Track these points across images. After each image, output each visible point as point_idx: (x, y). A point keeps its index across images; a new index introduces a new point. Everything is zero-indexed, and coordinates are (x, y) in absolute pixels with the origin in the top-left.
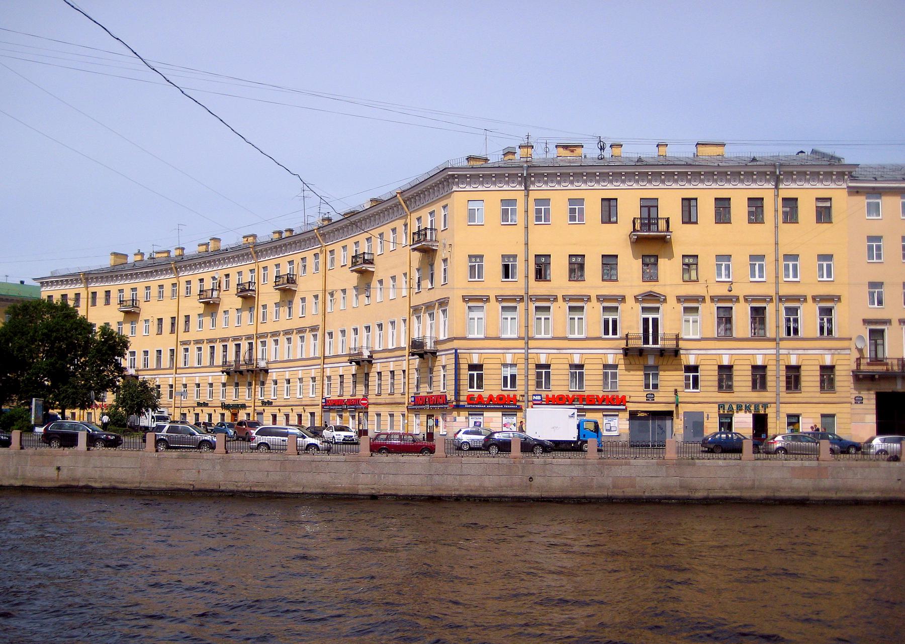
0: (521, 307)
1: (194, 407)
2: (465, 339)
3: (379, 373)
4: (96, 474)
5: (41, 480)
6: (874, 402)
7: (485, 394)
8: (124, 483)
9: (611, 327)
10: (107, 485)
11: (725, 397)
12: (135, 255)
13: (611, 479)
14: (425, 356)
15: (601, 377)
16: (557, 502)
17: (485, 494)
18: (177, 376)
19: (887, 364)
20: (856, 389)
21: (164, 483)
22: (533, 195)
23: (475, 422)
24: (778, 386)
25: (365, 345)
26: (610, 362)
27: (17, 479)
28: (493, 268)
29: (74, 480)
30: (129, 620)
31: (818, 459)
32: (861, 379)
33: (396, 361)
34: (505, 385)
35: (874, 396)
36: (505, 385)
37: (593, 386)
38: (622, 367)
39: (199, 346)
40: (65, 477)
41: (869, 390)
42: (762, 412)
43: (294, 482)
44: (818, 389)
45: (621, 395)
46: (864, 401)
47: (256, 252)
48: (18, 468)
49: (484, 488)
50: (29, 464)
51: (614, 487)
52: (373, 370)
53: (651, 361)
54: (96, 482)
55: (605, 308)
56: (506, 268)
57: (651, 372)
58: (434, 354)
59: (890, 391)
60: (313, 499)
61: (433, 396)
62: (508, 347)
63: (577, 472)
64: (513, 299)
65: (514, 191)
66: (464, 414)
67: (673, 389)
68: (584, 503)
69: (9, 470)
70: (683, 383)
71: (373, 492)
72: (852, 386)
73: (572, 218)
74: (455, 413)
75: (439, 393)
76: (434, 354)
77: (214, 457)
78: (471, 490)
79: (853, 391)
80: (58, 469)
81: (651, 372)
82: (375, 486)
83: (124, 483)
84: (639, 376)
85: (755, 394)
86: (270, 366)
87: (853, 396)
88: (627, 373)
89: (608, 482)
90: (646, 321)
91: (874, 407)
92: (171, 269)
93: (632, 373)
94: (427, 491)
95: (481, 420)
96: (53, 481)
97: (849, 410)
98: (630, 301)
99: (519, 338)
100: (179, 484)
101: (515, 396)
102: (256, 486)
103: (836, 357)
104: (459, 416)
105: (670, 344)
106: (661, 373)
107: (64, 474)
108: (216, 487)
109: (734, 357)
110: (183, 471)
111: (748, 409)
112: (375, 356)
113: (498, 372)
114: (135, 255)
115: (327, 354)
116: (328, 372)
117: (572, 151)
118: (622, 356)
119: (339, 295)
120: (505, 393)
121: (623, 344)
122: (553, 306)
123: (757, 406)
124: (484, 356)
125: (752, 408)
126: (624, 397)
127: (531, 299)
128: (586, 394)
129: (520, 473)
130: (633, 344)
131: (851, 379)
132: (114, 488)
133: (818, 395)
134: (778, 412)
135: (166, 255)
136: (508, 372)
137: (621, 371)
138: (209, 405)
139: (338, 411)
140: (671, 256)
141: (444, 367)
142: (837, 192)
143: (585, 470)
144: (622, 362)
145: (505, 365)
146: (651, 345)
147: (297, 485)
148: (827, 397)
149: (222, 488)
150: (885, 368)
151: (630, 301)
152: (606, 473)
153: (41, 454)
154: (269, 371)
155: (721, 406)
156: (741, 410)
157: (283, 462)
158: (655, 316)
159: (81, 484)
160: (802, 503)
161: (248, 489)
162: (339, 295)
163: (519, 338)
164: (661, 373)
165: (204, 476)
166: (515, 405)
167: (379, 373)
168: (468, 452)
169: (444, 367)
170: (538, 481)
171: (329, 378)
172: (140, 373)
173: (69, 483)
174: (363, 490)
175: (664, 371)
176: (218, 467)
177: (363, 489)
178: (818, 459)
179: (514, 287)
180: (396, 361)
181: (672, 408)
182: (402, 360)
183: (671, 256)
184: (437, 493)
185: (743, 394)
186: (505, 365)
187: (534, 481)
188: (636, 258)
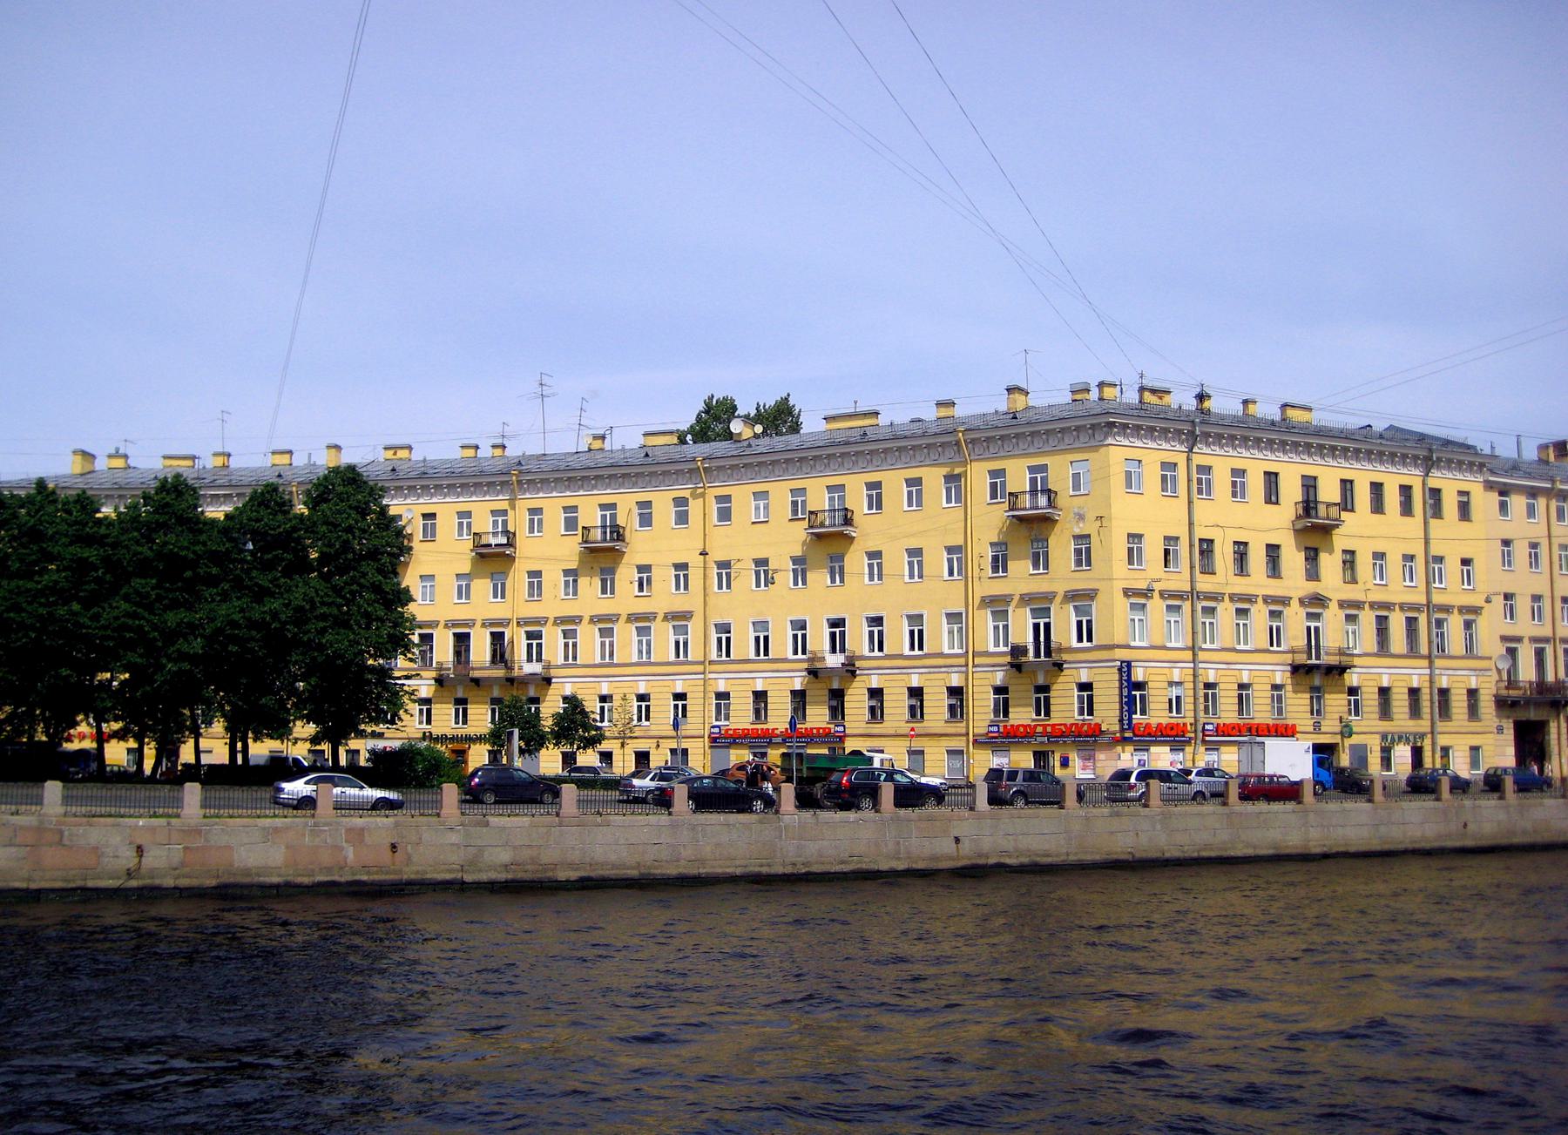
0: (1187, 606)
2: (1128, 647)
3: (876, 694)
4: (1008, 844)
5: (934, 858)
6: (1512, 731)
7: (1154, 721)
8: (1048, 856)
9: (1275, 636)
10: (1025, 860)
11: (1385, 726)
12: (110, 456)
15: (1236, 700)
16: (1265, 861)
17: (1428, 846)
19: (1520, 688)
20: (1498, 716)
21: (24, 880)
22: (1198, 460)
23: (1139, 761)
24: (1432, 714)
26: (1278, 681)
27: (899, 859)
28: (1153, 550)
29: (980, 856)
30: (461, 1103)
31: (558, 815)
32: (1502, 704)
33: (930, 673)
34: (1171, 710)
35: (1512, 725)
36: (1171, 710)
37: (1261, 713)
38: (1289, 688)
40: (967, 854)
41: (1508, 717)
42: (1419, 744)
43: (1243, 842)
44: (1466, 717)
45: (1290, 722)
46: (1505, 731)
47: (519, 482)
48: (898, 843)
49: (702, 861)
50: (914, 835)
51: (1535, 831)
53: (1317, 681)
54: (1010, 857)
55: (1169, 607)
57: (1317, 693)
59: (1524, 719)
61: (1049, 725)
62: (1229, 661)
63: (1502, 816)
64: (1179, 596)
65: (1174, 451)
66: (1130, 749)
67: (1337, 716)
68: (811, 881)
69: (886, 845)
70: (1346, 709)
71: (1325, 849)
72: (1494, 713)
73: (1234, 495)
74: (1119, 748)
75: (1072, 721)
77: (1153, 814)
78: (1415, 842)
79: (1495, 719)
80: (957, 840)
81: (1317, 693)
82: (1326, 842)
83: (1048, 856)
84: (1304, 698)
85: (1411, 723)
86: (553, 672)
87: (1495, 725)
88: (1294, 696)
89: (1528, 825)
90: (1309, 629)
91: (1512, 737)
93: (1299, 695)
94: (1376, 845)
95: (1146, 758)
96: (951, 858)
97: (1492, 741)
98: (1295, 604)
99: (1187, 649)
100: (1116, 853)
101: (1185, 724)
102: (1205, 850)
103: (1481, 679)
104: (1124, 752)
105: (1333, 660)
106: (1327, 696)
107: (966, 847)
108: (1158, 855)
109: (1393, 677)
110: (1119, 834)
111: (1408, 741)
113: (1165, 692)
114: (110, 456)
117: (1161, 398)
118: (1289, 674)
120: (1173, 721)
121: (1288, 658)
122: (1220, 607)
123: (1415, 735)
124: (1149, 671)
125: (1411, 738)
126: (1294, 726)
127: (1198, 597)
128: (1256, 721)
130: (1301, 659)
131: (1493, 705)
132: (1036, 865)
133: (1467, 723)
134: (1434, 744)
135: (189, 463)
136: (1175, 692)
137: (1288, 692)
138: (386, 735)
139: (751, 747)
140: (1331, 551)
142: (1474, 485)
144: (1289, 681)
145: (1171, 684)
146: (1314, 661)
147: (1248, 845)
148: (1475, 726)
149: (1167, 855)
150: (1521, 692)
151: (1295, 604)
153: (930, 819)
154: (554, 680)
155: (1384, 737)
157: (1229, 816)
158: (1317, 624)
159: (992, 861)
160: (1305, 858)
161: (1195, 855)
163: (1187, 649)
164: (1327, 696)
165: (1144, 840)
166: (1183, 736)
167: (876, 694)
168: (493, 806)
170: (1472, 827)
173: (974, 861)
174: (1316, 850)
175: (1330, 693)
177: (1315, 847)
178: (558, 815)
179: (1180, 582)
180: (930, 673)
181: (1337, 739)
182: (948, 673)
183: (1331, 551)
184: (1386, 847)
185: (1402, 723)
186: (1171, 684)
187: (1468, 827)
188: (1299, 550)
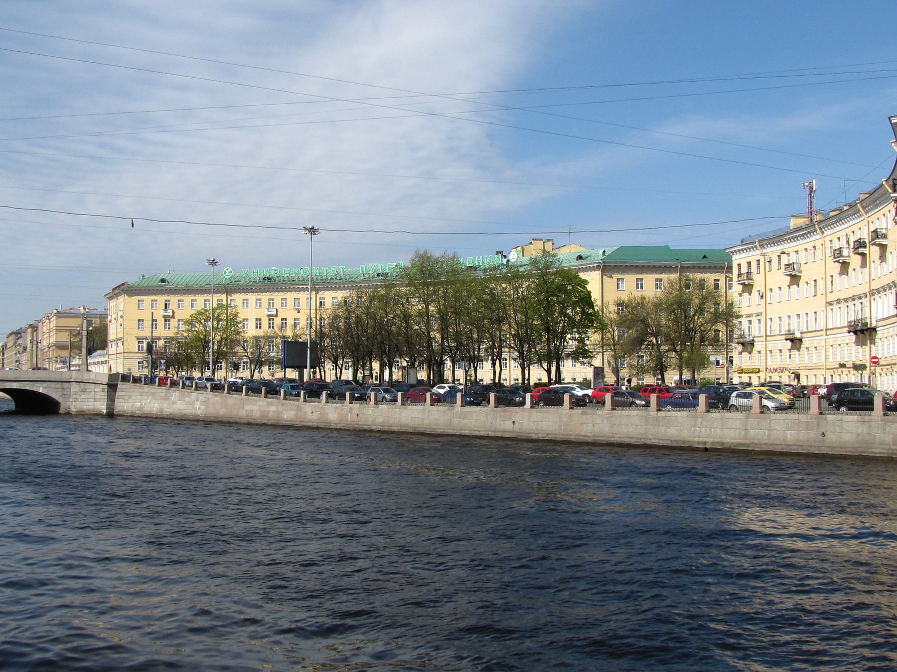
1: (837, 368)
13: (891, 436)
14: (795, 341)
18: (827, 337)
25: (796, 328)
39: (759, 318)
52: (754, 349)
56: (166, 305)
58: (800, 340)
60: (390, 439)
76: (800, 340)
78: (597, 436)
92: (756, 247)
96: (511, 432)
112: (756, 339)
115: (768, 334)
116: (769, 347)
119: (776, 290)
129: (815, 428)
141: (807, 348)
143: (870, 427)
152: (887, 430)
156: (166, 384)
162: (776, 290)
169: (807, 348)
171: (771, 351)
172: (804, 335)
176: (605, 422)
187: (826, 436)
